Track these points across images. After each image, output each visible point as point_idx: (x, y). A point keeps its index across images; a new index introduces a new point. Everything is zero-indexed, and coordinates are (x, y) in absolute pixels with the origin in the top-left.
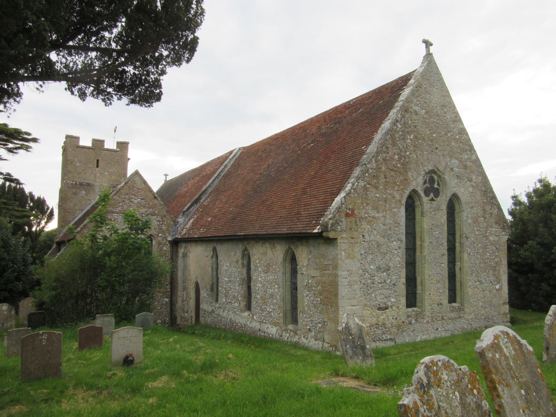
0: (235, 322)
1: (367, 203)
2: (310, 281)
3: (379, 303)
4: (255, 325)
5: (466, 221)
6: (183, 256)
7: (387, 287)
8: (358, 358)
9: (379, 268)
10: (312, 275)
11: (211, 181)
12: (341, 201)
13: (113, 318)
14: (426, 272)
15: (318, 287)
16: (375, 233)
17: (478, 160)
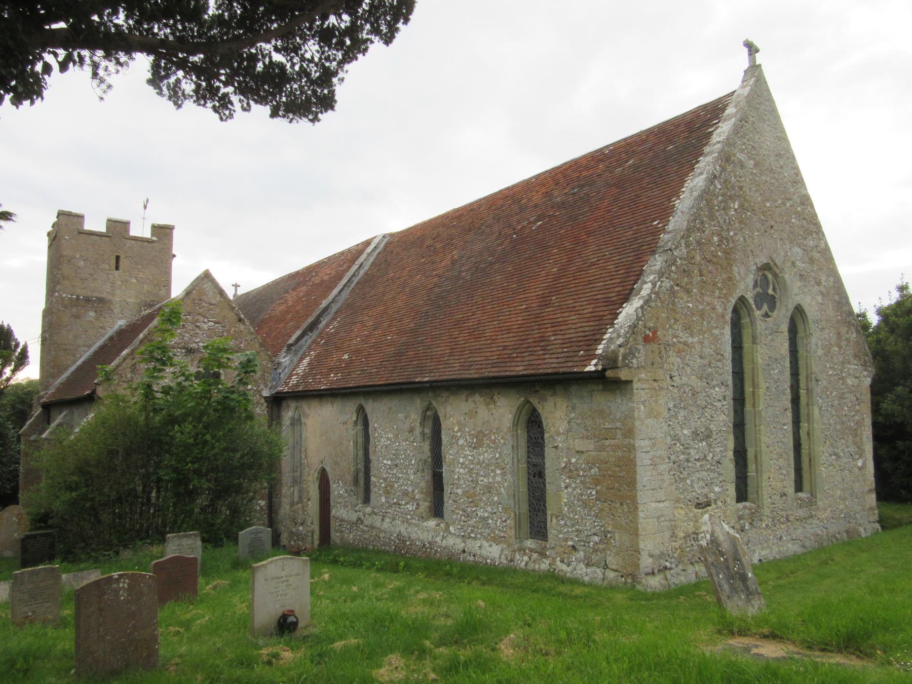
0: (409, 538)
1: (675, 319)
2: (573, 460)
3: (698, 496)
4: (453, 543)
5: (815, 352)
6: (292, 424)
7: (709, 467)
8: (740, 597)
9: (695, 434)
10: (578, 449)
11: (335, 292)
12: (637, 315)
13: (199, 539)
14: (763, 439)
15: (593, 471)
16: (689, 371)
17: (827, 250)
